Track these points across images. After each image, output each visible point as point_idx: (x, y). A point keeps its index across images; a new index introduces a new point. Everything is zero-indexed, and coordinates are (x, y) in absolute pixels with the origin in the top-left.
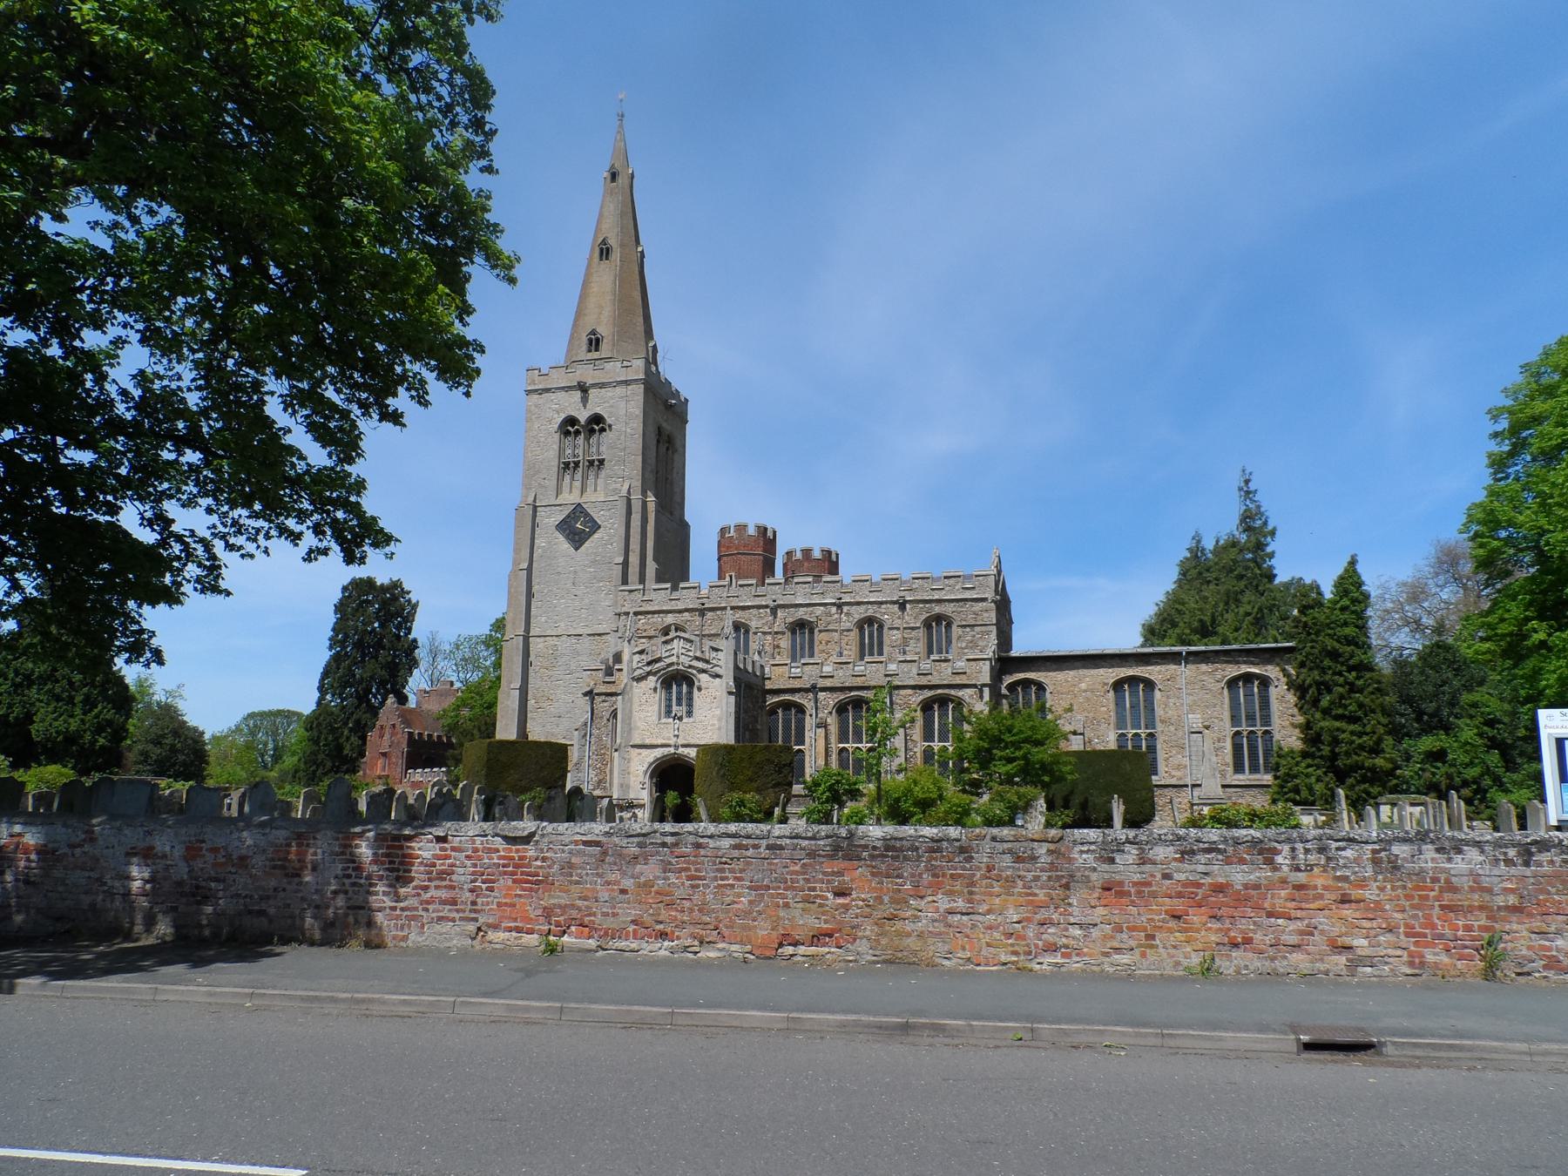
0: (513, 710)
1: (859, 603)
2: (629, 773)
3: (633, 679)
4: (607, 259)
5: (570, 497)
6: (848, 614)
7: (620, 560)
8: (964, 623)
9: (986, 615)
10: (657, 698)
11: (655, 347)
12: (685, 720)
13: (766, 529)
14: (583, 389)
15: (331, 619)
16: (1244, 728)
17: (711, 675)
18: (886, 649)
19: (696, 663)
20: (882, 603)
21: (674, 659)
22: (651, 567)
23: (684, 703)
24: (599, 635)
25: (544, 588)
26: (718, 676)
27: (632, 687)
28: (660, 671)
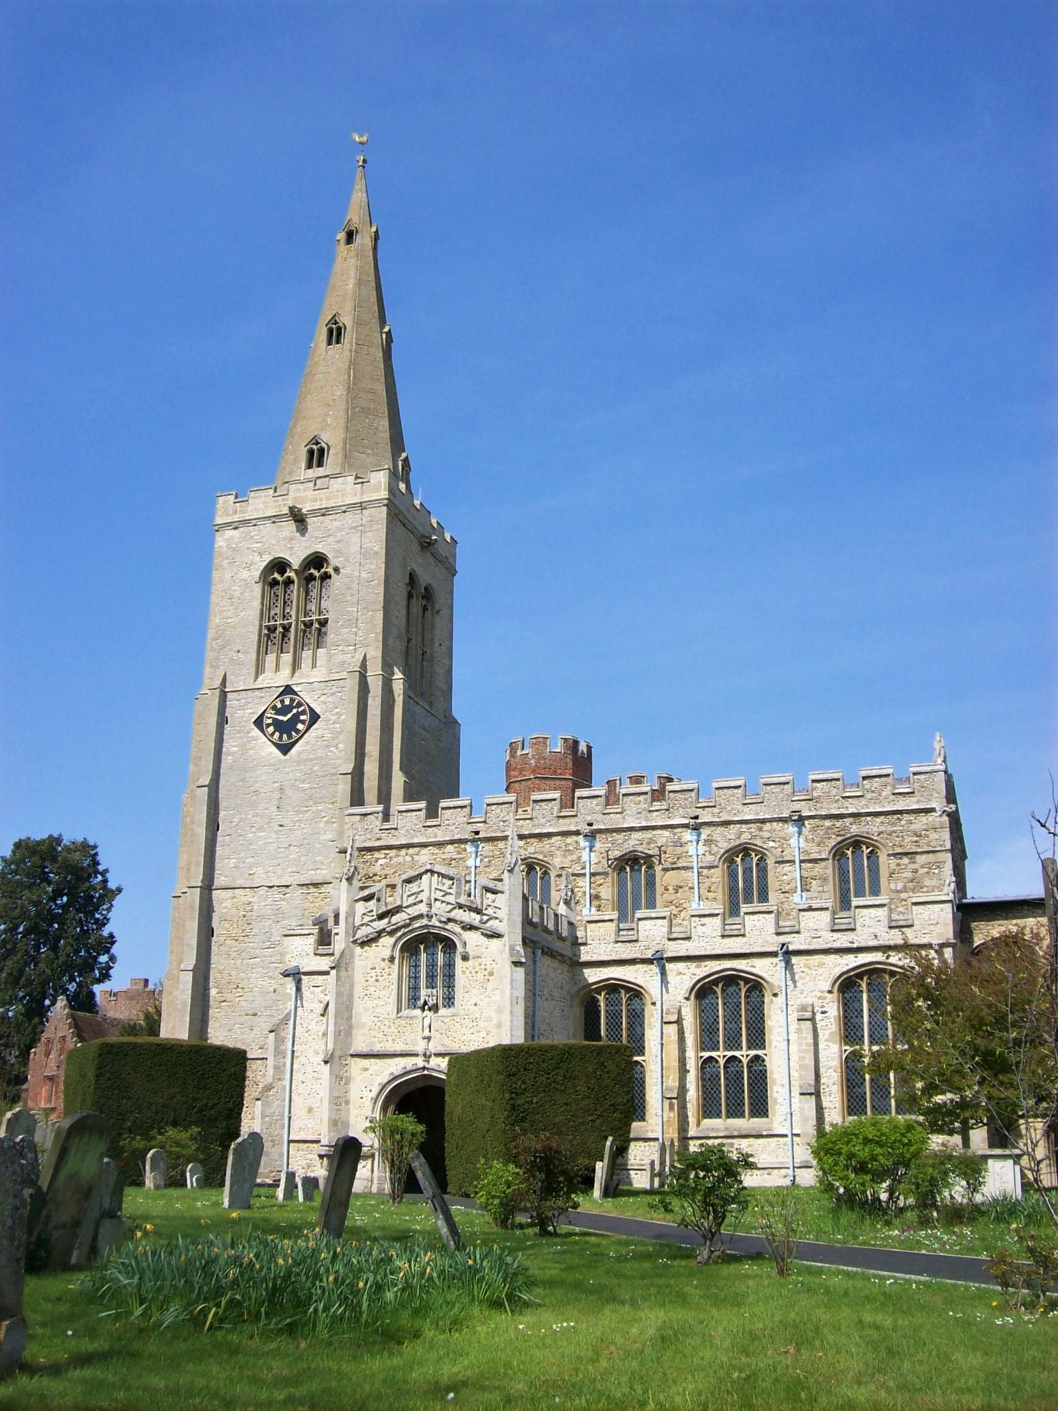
0: (184, 1003)
1: (726, 823)
2: (347, 1102)
3: (355, 942)
4: (338, 342)
5: (277, 676)
6: (709, 842)
7: (349, 767)
8: (899, 850)
9: (933, 836)
11: (406, 461)
12: (442, 1011)
13: (576, 743)
14: (299, 518)
16: (721, 1055)
17: (482, 934)
18: (772, 896)
19: (459, 914)
20: (763, 821)
21: (423, 908)
22: (398, 780)
23: (439, 982)
24: (316, 885)
25: (233, 816)
26: (499, 936)
27: (352, 955)
28: (398, 929)
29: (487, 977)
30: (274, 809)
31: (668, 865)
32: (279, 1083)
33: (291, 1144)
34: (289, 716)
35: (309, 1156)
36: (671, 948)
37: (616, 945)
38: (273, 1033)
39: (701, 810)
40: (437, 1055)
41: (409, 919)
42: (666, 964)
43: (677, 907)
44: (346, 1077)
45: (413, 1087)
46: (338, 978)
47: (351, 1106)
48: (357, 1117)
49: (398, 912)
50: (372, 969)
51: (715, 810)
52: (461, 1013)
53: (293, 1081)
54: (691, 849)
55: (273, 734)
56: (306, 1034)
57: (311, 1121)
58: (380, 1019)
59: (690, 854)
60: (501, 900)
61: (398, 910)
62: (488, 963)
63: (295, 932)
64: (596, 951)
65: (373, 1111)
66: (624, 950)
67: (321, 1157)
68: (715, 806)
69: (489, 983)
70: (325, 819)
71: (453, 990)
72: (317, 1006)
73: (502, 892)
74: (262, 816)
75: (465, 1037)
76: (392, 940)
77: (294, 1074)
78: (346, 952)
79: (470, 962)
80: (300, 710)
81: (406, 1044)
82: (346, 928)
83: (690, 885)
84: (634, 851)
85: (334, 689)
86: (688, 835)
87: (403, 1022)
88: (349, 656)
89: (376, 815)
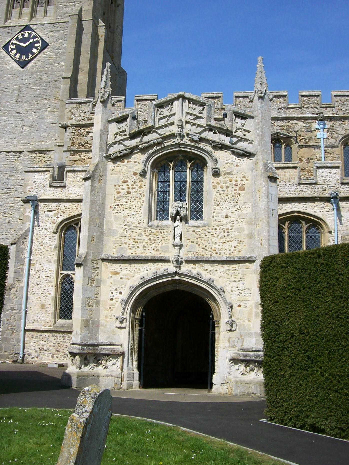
2: (98, 303)
3: (108, 157)
6: (330, 130)
10: (146, 188)
15: (5, 302)
17: (234, 153)
19: (209, 135)
21: (175, 129)
24: (41, 152)
26: (248, 155)
27: (105, 169)
28: (151, 146)
29: (238, 192)
30: (14, 102)
31: (302, 144)
32: (18, 284)
33: (27, 333)
34: (28, 44)
35: (42, 342)
36: (344, 190)
37: (299, 187)
38: (15, 246)
39: (324, 109)
40: (188, 262)
41: (162, 138)
42: (340, 202)
43: (309, 173)
44: (97, 279)
45: (161, 291)
46: (93, 187)
47: (101, 307)
48: (107, 317)
49: (149, 133)
50: (123, 182)
51: (335, 110)
52: (213, 224)
53: (30, 283)
54: (319, 134)
55: (16, 55)
56: (41, 247)
57: (44, 315)
58: (132, 227)
59: (318, 137)
60: (249, 124)
61: (150, 130)
62: (239, 179)
63: (34, 169)
64: (283, 190)
65: (124, 312)
66: (305, 190)
67: (73, 355)
68: (334, 107)
69: (241, 198)
70: (49, 109)
71: (200, 204)
72: (51, 226)
73: (252, 117)
74: (5, 106)
75: (217, 246)
76: (144, 157)
77: (30, 278)
78: (100, 165)
79: (221, 178)
80: (35, 40)
81: (158, 251)
82: (101, 145)
83: (318, 158)
84: (278, 133)
85: (59, 28)
86: (316, 125)
87: (153, 230)
88: (70, 9)
89: (88, 104)
